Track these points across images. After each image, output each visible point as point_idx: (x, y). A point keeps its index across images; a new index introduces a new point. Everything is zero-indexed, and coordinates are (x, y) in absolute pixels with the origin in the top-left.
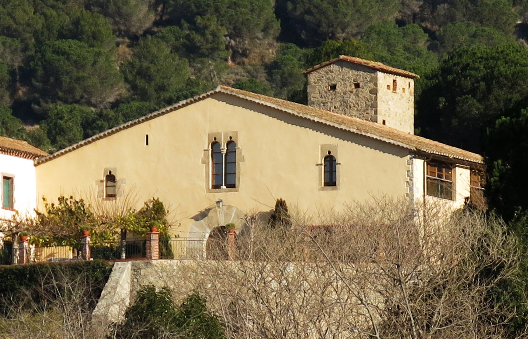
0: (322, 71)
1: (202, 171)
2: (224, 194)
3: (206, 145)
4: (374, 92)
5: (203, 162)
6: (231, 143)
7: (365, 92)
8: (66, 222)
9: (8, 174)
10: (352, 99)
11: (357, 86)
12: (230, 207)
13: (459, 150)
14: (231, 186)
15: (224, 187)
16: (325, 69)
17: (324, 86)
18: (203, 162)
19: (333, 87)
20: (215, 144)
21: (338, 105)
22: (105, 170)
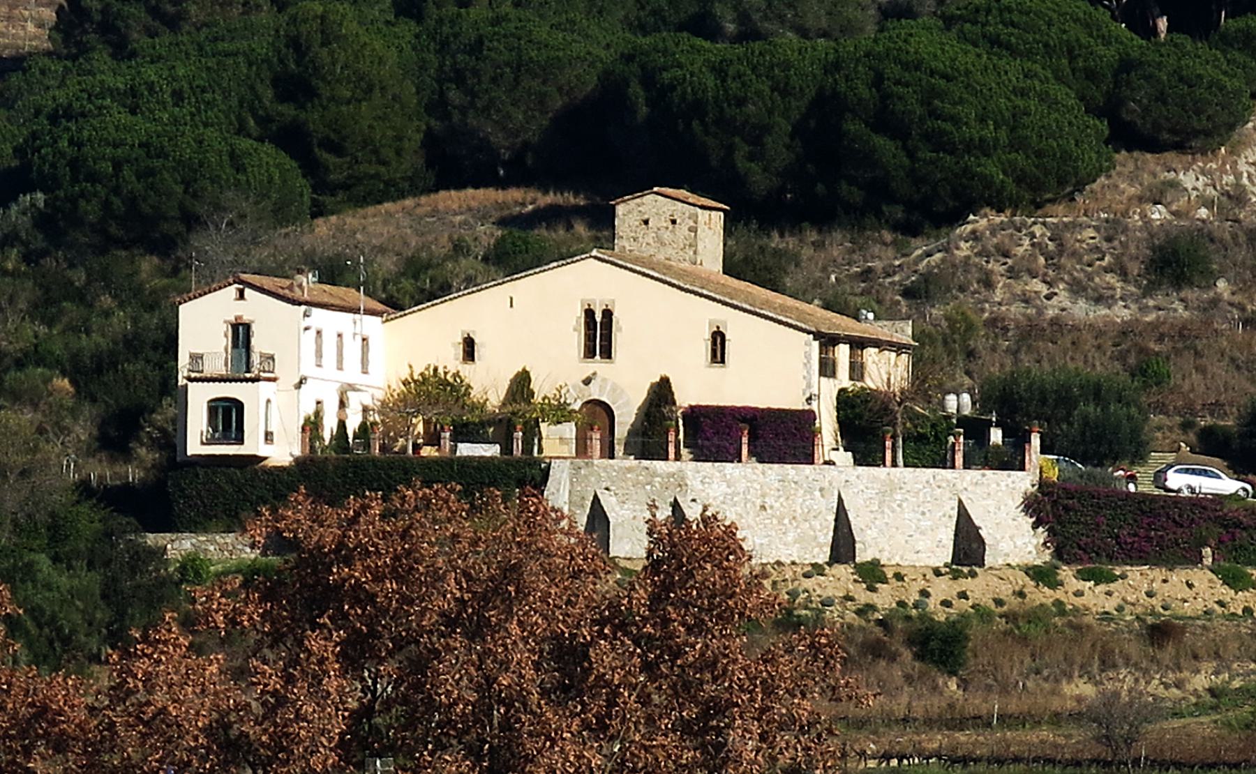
0: (632, 203)
1: (575, 340)
2: (597, 365)
3: (708, 336)
4: (693, 230)
5: (575, 330)
6: (608, 314)
7: (683, 230)
8: (435, 395)
9: (340, 331)
10: (667, 236)
11: (674, 222)
12: (604, 380)
13: (217, 453)
14: (607, 353)
15: (598, 357)
16: (638, 200)
17: (634, 220)
18: (575, 330)
19: (646, 222)
20: (589, 313)
21: (651, 241)
22: (463, 332)
